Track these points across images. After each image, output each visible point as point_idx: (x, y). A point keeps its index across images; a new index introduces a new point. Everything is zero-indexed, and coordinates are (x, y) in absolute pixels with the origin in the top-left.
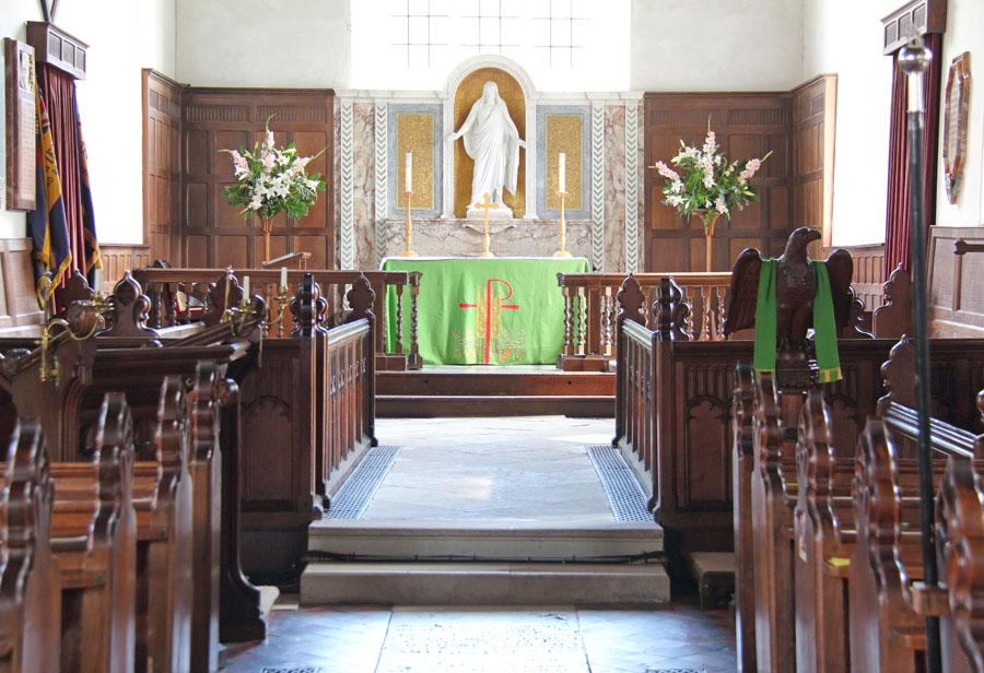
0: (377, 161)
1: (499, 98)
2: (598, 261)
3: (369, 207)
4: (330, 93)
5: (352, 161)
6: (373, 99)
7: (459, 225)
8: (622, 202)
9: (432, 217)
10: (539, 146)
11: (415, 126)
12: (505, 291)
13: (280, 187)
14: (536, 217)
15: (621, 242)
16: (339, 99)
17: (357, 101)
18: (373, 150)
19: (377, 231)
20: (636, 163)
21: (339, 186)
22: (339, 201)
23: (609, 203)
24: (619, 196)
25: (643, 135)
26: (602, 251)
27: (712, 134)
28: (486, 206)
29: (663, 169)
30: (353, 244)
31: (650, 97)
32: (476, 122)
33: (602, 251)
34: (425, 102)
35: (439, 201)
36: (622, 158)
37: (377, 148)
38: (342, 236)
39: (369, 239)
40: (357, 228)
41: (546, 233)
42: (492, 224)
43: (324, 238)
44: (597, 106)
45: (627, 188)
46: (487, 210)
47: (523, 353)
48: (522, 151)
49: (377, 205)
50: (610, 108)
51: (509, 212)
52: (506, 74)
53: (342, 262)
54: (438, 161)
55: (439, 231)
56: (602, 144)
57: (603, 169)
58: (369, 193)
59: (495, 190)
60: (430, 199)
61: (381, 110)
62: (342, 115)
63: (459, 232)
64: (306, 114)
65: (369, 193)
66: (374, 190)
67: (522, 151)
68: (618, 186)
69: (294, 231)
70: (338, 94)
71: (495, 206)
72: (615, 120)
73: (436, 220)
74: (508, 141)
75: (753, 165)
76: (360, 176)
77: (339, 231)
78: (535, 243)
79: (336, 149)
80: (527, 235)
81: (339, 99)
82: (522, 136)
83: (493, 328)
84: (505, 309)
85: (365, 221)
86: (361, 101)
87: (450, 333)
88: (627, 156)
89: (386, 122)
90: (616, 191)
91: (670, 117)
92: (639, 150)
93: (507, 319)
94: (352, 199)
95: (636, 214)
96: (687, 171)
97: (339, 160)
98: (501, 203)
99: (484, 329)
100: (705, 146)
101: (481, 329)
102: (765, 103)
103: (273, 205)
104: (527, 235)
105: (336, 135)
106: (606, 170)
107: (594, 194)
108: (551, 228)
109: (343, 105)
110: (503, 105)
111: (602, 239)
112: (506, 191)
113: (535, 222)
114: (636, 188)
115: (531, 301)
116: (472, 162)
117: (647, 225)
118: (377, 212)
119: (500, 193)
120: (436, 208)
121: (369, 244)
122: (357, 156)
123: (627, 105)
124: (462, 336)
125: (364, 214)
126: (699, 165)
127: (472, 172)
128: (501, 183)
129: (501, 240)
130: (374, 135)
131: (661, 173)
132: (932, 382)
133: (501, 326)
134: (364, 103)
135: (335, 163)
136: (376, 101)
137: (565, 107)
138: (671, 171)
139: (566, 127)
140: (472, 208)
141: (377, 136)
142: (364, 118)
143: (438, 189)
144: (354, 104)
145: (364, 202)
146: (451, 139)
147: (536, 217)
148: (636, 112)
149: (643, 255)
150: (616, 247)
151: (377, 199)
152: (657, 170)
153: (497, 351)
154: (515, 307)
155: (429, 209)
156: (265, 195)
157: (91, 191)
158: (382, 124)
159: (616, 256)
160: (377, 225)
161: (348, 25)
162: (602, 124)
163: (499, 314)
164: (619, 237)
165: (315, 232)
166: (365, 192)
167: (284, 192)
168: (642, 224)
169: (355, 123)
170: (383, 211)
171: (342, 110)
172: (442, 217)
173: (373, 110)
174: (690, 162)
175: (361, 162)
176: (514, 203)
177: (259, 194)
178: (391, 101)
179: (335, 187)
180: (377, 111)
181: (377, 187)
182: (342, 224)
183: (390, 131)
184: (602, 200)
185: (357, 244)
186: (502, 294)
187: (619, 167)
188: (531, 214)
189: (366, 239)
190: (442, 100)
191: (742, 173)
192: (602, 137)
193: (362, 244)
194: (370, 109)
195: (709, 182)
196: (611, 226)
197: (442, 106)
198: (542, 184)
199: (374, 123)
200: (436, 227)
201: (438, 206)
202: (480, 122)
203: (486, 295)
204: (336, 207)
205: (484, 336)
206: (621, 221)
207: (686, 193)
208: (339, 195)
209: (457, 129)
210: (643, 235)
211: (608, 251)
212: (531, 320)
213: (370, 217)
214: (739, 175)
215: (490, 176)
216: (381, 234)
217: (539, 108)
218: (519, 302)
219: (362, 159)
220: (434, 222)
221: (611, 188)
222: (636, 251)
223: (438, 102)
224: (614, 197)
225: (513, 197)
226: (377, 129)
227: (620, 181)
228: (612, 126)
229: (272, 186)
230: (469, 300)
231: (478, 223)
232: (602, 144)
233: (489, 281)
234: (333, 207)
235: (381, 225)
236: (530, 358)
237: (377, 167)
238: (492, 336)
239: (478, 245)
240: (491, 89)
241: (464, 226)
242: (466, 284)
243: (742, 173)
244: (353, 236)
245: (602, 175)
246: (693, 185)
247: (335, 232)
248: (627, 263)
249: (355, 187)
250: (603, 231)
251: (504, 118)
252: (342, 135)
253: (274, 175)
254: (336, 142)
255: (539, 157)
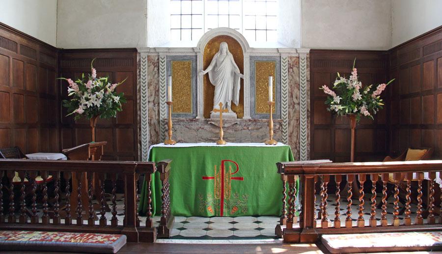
0: (160, 87)
1: (228, 51)
2: (285, 138)
3: (157, 112)
4: (135, 50)
5: (147, 87)
6: (158, 53)
7: (206, 122)
8: (298, 109)
9: (191, 118)
10: (251, 78)
11: (181, 64)
12: (234, 169)
13: (95, 101)
14: (250, 118)
15: (297, 131)
16: (140, 53)
17: (149, 54)
18: (159, 81)
19: (161, 126)
20: (306, 88)
21: (140, 102)
22: (140, 109)
23: (291, 110)
24: (296, 106)
25: (309, 73)
26: (287, 136)
27: (355, 70)
28: (222, 111)
29: (327, 90)
30: (148, 132)
31: (313, 52)
32: (216, 65)
33: (287, 136)
34: (187, 54)
35: (195, 109)
36: (298, 85)
37: (160, 80)
38: (142, 129)
39: (156, 130)
40: (150, 124)
41: (256, 127)
42: (224, 122)
43: (132, 130)
44: (283, 56)
45: (301, 102)
46: (221, 114)
47: (246, 209)
48: (242, 80)
49: (160, 111)
50: (291, 58)
51: (235, 115)
52: (232, 38)
53: (142, 142)
54: (194, 87)
55: (194, 126)
56: (287, 77)
57: (287, 91)
58: (156, 105)
59: (227, 103)
60: (169, 129)
61: (163, 59)
62: (141, 62)
63: (206, 126)
64: (121, 62)
65: (156, 105)
66: (159, 103)
67: (242, 80)
68: (296, 101)
69: (117, 126)
70: (139, 51)
71: (227, 111)
72: (294, 64)
73: (194, 120)
74: (234, 75)
75: (381, 87)
76: (151, 95)
77: (140, 126)
78: (250, 132)
79: (138, 81)
80: (245, 128)
81: (140, 53)
82: (242, 72)
83: (226, 193)
84: (234, 180)
85: (154, 121)
86: (153, 54)
87: (196, 195)
88: (301, 84)
89: (166, 66)
90: (294, 103)
91: (324, 63)
92: (307, 81)
93: (235, 187)
94: (147, 108)
95: (306, 116)
96: (343, 91)
97: (140, 87)
98: (230, 111)
99: (219, 193)
100: (351, 76)
101: (218, 193)
102: (342, 56)
103: (93, 111)
104: (245, 128)
105: (138, 74)
106: (289, 92)
107: (282, 105)
108: (259, 124)
109: (142, 57)
110: (231, 56)
111: (287, 129)
112: (233, 104)
113: (250, 120)
114: (306, 102)
115: (251, 174)
116: (214, 87)
117: (312, 123)
118: (161, 115)
119: (229, 104)
120: (193, 113)
121: (157, 133)
122: (150, 85)
123: (300, 56)
124: (205, 198)
125: (154, 116)
126: (350, 87)
127: (214, 93)
128: (230, 98)
129: (230, 131)
130: (159, 73)
131: (326, 92)
132: (273, 98)
133: (231, 191)
134: (153, 55)
135: (138, 88)
136: (160, 54)
137: (266, 57)
138: (331, 91)
139: (266, 66)
140: (213, 113)
141: (160, 73)
142: (154, 64)
143: (195, 103)
144: (148, 56)
145: (154, 110)
146: (201, 74)
147: (250, 118)
148: (305, 60)
149: (309, 138)
150: (295, 134)
151: (161, 108)
152: (323, 90)
153: (228, 207)
154: (241, 179)
155: (189, 114)
156: (86, 105)
157: (390, 49)
158: (163, 66)
159: (295, 139)
160: (161, 122)
161: (146, 15)
162: (287, 66)
163: (229, 183)
164: (296, 128)
165: (128, 126)
166: (154, 104)
167: (98, 103)
168: (309, 121)
169: (149, 66)
170: (164, 115)
171: (141, 59)
172: (197, 118)
173: (158, 59)
174: (344, 85)
175: (152, 88)
176: (237, 110)
177: (82, 104)
178: (168, 54)
179: (138, 101)
180: (160, 59)
181: (160, 101)
182: (142, 122)
183: (167, 70)
184: (287, 108)
185: (150, 133)
186: (231, 171)
187: (296, 90)
188: (247, 116)
189: (155, 130)
190: (196, 53)
191: (374, 92)
192: (287, 74)
193: (153, 133)
194: (156, 58)
195: (357, 96)
196: (292, 123)
197: (196, 56)
198: (253, 99)
199: (159, 66)
200: (193, 123)
201: (195, 112)
202: (218, 65)
203: (221, 171)
204: (138, 113)
205: (220, 198)
206: (297, 120)
207: (342, 103)
208: (140, 106)
209: (205, 68)
210: (309, 127)
211: (290, 136)
212: (252, 187)
213: (157, 118)
214: (372, 93)
215: (223, 94)
216: (163, 128)
217: (251, 58)
218: (244, 175)
219: (152, 86)
220: (192, 120)
221: (292, 102)
222: (306, 137)
223: (194, 54)
224: (294, 107)
225: (237, 106)
226: (160, 70)
227: (296, 98)
228: (292, 68)
229: (90, 99)
230: (209, 175)
231: (217, 121)
232: (287, 77)
233: (223, 162)
234: (137, 112)
235: (163, 122)
236: (251, 212)
237: (160, 91)
238: (225, 198)
239: (218, 133)
240: (225, 46)
241: (209, 123)
242: (206, 163)
243: (374, 92)
244: (148, 129)
245: (287, 94)
246: (347, 100)
247: (138, 127)
248: (301, 143)
249: (149, 102)
250: (287, 126)
251: (231, 61)
252: (141, 73)
253: (93, 92)
254: (138, 77)
255: (252, 85)
